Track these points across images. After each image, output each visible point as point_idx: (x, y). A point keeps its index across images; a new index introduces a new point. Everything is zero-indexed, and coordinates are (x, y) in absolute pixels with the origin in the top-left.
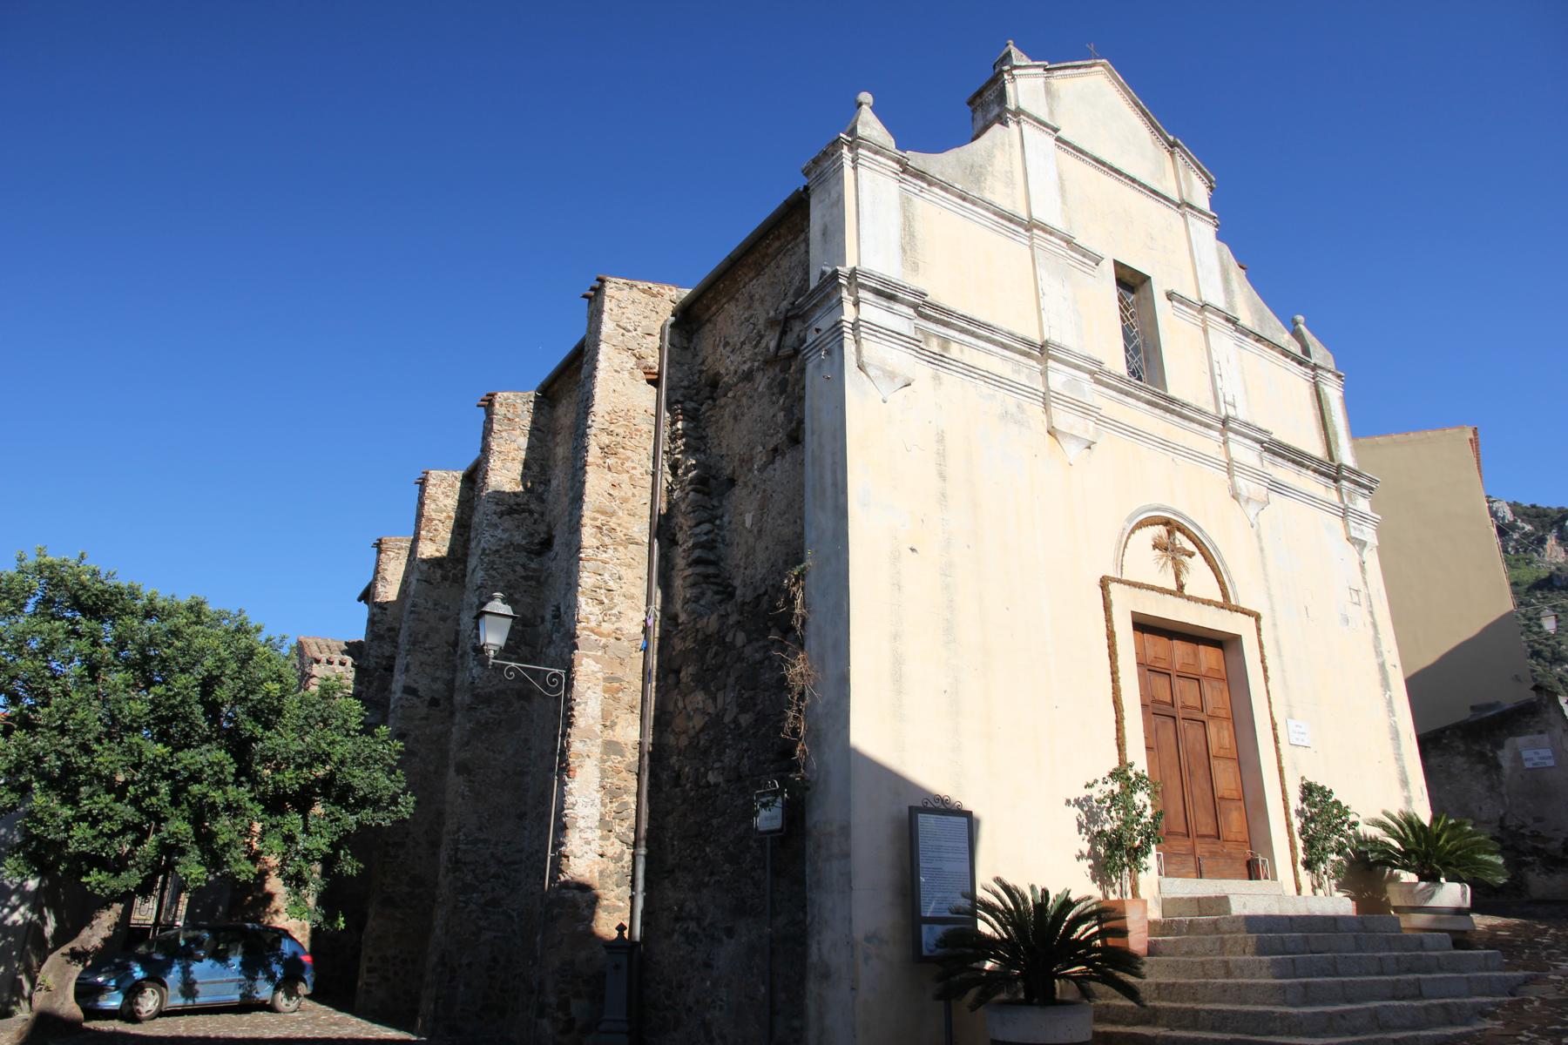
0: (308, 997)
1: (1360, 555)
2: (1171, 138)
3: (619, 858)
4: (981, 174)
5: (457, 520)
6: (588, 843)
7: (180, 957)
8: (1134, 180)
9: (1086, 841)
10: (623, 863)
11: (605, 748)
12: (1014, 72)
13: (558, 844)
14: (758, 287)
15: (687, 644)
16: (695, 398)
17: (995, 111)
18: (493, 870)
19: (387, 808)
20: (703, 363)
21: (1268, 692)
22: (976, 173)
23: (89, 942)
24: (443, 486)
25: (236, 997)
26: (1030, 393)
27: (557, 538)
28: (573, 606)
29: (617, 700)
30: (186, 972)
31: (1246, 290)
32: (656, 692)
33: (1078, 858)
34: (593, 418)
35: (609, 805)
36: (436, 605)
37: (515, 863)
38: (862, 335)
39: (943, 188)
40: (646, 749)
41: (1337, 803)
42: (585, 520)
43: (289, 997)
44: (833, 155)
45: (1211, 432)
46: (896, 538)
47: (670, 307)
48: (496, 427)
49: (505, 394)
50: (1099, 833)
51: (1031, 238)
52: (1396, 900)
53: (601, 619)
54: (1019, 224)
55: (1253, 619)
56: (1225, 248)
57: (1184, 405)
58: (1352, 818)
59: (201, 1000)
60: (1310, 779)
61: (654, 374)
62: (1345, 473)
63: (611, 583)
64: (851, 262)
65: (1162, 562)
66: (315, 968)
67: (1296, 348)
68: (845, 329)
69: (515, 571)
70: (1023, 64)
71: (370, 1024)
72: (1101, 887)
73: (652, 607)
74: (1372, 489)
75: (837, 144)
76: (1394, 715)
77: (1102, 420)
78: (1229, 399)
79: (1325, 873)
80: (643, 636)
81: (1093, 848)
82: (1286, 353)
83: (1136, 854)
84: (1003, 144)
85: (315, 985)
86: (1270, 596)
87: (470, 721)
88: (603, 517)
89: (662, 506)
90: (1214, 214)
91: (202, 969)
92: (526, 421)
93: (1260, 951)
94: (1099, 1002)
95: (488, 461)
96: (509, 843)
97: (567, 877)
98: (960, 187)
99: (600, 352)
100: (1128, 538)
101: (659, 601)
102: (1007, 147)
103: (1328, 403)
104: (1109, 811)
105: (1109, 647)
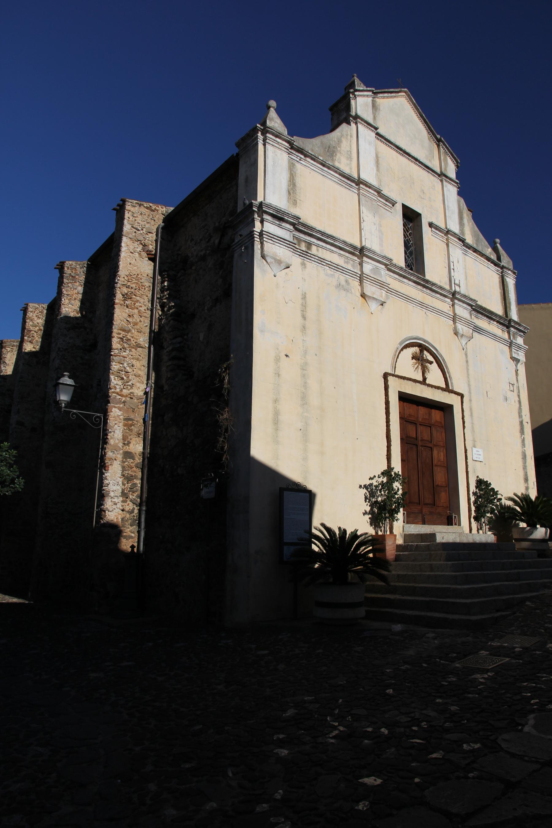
1: (516, 366)
2: (439, 136)
3: (132, 512)
4: (334, 152)
6: (115, 504)
8: (416, 160)
9: (368, 506)
11: (124, 456)
12: (356, 93)
13: (100, 504)
17: (344, 115)
19: (9, 486)
21: (464, 434)
22: (331, 151)
24: (36, 313)
26: (353, 274)
28: (108, 380)
29: (131, 430)
31: (471, 224)
32: (152, 426)
33: (364, 514)
34: (118, 278)
35: (127, 485)
38: (265, 239)
39: (313, 159)
40: (146, 456)
41: (493, 489)
42: (114, 334)
44: (253, 136)
45: (446, 299)
46: (278, 349)
47: (162, 217)
48: (65, 281)
49: (70, 262)
50: (375, 502)
51: (359, 189)
52: (516, 536)
53: (122, 387)
54: (353, 181)
55: (460, 397)
56: (462, 201)
57: (434, 284)
58: (499, 496)
60: (481, 477)
61: (152, 255)
62: (512, 324)
63: (128, 368)
64: (260, 199)
65: (416, 366)
67: (494, 257)
68: (255, 236)
70: (361, 89)
71: (3, 596)
72: (374, 528)
73: (150, 381)
74: (525, 332)
75: (255, 130)
76: (525, 447)
77: (390, 291)
78: (457, 282)
79: (484, 522)
81: (372, 509)
82: (488, 259)
83: (392, 513)
84: (347, 135)
86: (469, 385)
88: (124, 333)
89: (156, 327)
90: (457, 181)
92: (82, 278)
93: (448, 559)
94: (368, 583)
95: (61, 300)
97: (105, 521)
98: (322, 159)
99: (123, 241)
100: (399, 353)
101: (153, 378)
102: (349, 137)
103: (508, 287)
104: (380, 492)
105: (386, 409)
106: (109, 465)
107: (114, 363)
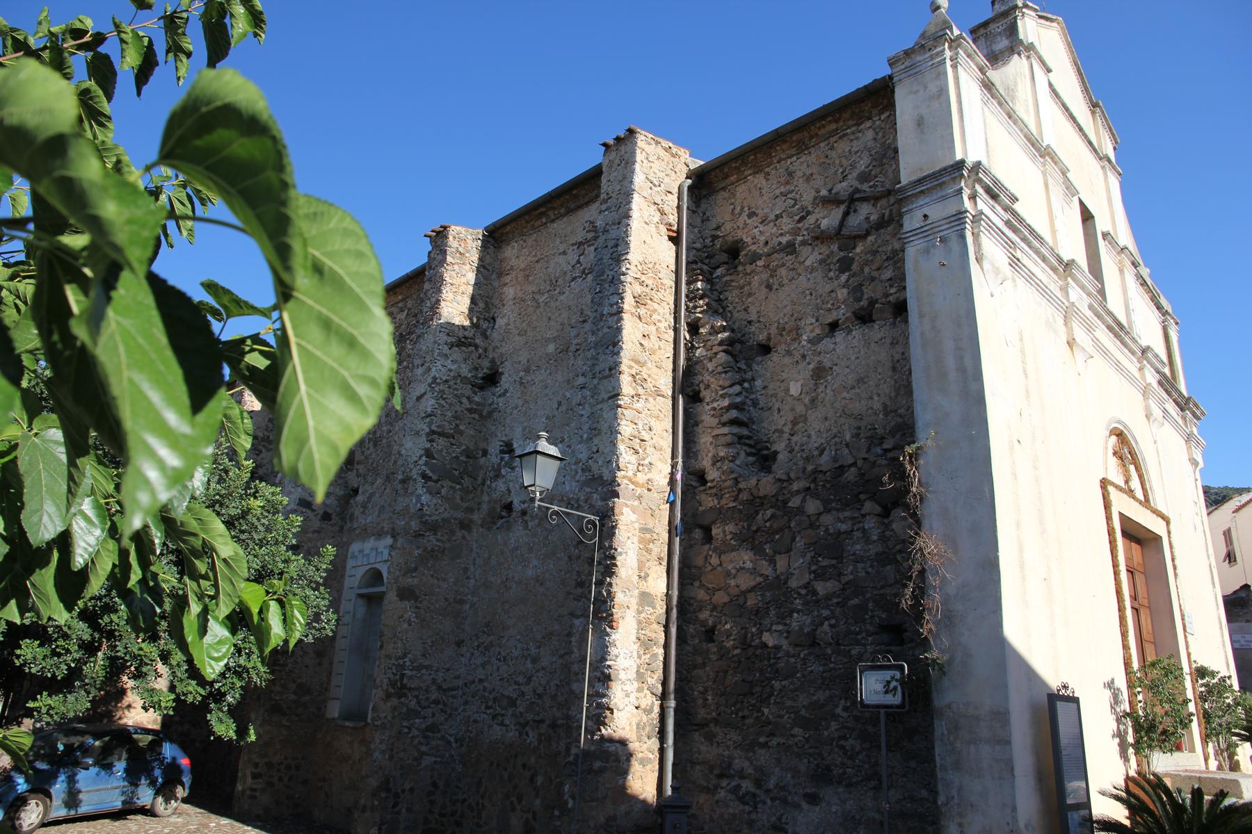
0: (185, 801)
3: (648, 711)
7: (65, 765)
10: (653, 715)
14: (801, 165)
15: (724, 501)
16: (707, 261)
18: (433, 696)
20: (718, 228)
25: (118, 805)
27: (506, 375)
29: (649, 551)
35: (643, 657)
37: (453, 689)
38: (982, 229)
43: (167, 801)
44: (930, 50)
49: (458, 228)
59: (83, 809)
61: (673, 231)
68: (967, 220)
69: (461, 403)
80: (668, 489)
87: (418, 548)
88: (637, 367)
91: (87, 778)
92: (474, 257)
96: (448, 670)
106: (618, 619)
107: (623, 422)
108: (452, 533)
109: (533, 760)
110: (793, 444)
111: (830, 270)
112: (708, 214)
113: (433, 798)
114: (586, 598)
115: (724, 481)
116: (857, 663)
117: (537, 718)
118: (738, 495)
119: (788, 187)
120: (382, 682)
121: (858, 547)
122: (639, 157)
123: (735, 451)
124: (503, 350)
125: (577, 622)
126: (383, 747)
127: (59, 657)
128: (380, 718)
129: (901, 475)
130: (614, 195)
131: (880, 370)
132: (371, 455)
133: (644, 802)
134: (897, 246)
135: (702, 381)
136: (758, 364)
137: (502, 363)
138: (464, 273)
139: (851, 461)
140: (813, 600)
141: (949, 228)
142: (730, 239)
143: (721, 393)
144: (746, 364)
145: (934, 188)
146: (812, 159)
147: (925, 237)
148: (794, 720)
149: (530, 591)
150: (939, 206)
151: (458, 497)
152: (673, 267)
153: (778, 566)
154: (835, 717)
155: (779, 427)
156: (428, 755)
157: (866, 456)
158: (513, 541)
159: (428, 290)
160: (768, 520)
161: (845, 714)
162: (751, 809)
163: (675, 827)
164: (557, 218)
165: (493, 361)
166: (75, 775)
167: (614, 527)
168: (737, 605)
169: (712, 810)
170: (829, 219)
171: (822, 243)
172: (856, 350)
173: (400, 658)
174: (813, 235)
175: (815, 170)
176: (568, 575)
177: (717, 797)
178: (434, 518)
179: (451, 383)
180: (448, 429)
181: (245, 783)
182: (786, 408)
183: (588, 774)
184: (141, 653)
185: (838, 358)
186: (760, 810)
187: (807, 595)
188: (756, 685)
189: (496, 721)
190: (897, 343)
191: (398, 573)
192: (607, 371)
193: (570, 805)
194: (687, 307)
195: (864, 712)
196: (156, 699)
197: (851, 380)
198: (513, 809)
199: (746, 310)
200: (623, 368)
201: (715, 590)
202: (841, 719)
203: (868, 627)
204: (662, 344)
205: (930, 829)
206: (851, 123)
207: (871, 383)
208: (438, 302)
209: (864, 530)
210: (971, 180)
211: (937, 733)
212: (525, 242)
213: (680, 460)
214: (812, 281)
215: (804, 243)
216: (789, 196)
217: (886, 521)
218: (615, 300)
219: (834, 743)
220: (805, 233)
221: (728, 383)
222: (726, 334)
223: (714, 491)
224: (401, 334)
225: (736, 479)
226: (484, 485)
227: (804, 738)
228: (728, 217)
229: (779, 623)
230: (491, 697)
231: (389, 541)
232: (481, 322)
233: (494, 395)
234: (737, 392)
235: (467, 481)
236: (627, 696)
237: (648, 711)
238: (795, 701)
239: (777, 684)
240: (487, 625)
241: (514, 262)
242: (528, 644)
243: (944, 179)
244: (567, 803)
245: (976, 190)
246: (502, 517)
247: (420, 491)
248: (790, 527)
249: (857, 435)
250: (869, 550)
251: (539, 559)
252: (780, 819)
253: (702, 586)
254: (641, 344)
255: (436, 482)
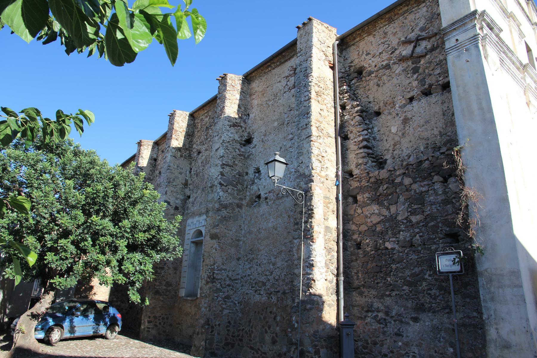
0: (120, 333)
3: (331, 282)
5: (186, 133)
7: (68, 315)
14: (390, 29)
15: (362, 183)
16: (347, 78)
18: (228, 283)
20: (352, 62)
23: (40, 310)
24: (181, 117)
25: (91, 333)
27: (255, 138)
29: (328, 208)
30: (71, 321)
35: (328, 256)
36: (178, 167)
37: (236, 280)
43: (112, 332)
49: (231, 75)
59: (77, 334)
66: (122, 320)
68: (479, 38)
69: (236, 152)
85: (122, 327)
87: (219, 216)
88: (319, 123)
91: (78, 320)
92: (239, 87)
96: (234, 271)
107: (314, 148)
108: (234, 209)
109: (275, 309)
110: (395, 155)
111: (408, 74)
112: (346, 57)
113: (229, 328)
114: (299, 229)
115: (362, 174)
116: (435, 253)
117: (276, 290)
118: (369, 180)
119: (385, 39)
120: (204, 276)
121: (432, 198)
122: (315, 30)
123: (367, 160)
124: (253, 128)
125: (295, 241)
126: (206, 305)
127: (63, 261)
128: (204, 293)
129: (452, 161)
130: (303, 49)
131: (436, 116)
132: (195, 180)
133: (330, 325)
134: (442, 58)
135: (349, 130)
136: (375, 120)
137: (253, 133)
138: (235, 94)
139: (425, 158)
140: (410, 224)
141: (470, 44)
142: (358, 66)
143: (358, 134)
144: (369, 121)
145: (460, 26)
146: (396, 25)
147: (457, 50)
148: (403, 282)
149: (270, 233)
150: (464, 34)
151: (236, 193)
152: (332, 80)
153: (391, 210)
154: (425, 280)
155: (387, 148)
156: (226, 309)
157: (433, 155)
158: (261, 211)
159: (219, 103)
160: (385, 190)
161: (430, 278)
162: (384, 326)
163: (348, 335)
164: (276, 67)
165: (249, 133)
166: (73, 319)
167: (312, 196)
168: (372, 231)
169: (364, 328)
170: (406, 51)
171: (403, 62)
172: (424, 108)
173: (212, 265)
174: (399, 59)
175: (397, 29)
176: (288, 224)
177: (366, 321)
178: (225, 202)
179: (231, 143)
180: (230, 163)
181: (145, 325)
182: (390, 139)
183: (304, 311)
184: (98, 259)
185: (415, 113)
186: (388, 326)
187: (407, 223)
188: (383, 267)
189: (257, 293)
190: (444, 103)
191: (210, 228)
192: (305, 126)
193: (296, 325)
194: (340, 98)
195: (441, 276)
196: (105, 279)
197: (422, 122)
198: (266, 332)
199: (367, 97)
200: (312, 123)
201: (360, 225)
202: (428, 281)
203: (440, 235)
204: (329, 114)
205: (480, 331)
206: (415, 5)
207: (432, 122)
208: (224, 107)
209: (434, 189)
210: (480, 20)
211: (480, 284)
212: (261, 79)
213: (340, 166)
214: (399, 80)
215: (394, 63)
216: (386, 43)
217: (445, 184)
218: (307, 94)
219: (425, 292)
220: (395, 59)
221: (361, 129)
222: (359, 108)
223: (357, 179)
224: (207, 127)
225: (368, 173)
226: (247, 188)
227: (409, 291)
228: (356, 57)
229: (393, 237)
230: (254, 282)
231: (204, 217)
232: (243, 116)
233: (250, 148)
234: (366, 134)
235: (239, 186)
236: (321, 274)
237: (331, 282)
238: (403, 273)
239: (394, 266)
240: (251, 250)
241: (257, 89)
242: (270, 257)
243: (466, 21)
244: (294, 325)
245: (483, 25)
246: (256, 202)
247: (219, 191)
248: (396, 192)
249: (427, 147)
250: (438, 198)
251: (274, 218)
252: (399, 330)
253: (354, 223)
254: (320, 114)
255: (226, 186)
